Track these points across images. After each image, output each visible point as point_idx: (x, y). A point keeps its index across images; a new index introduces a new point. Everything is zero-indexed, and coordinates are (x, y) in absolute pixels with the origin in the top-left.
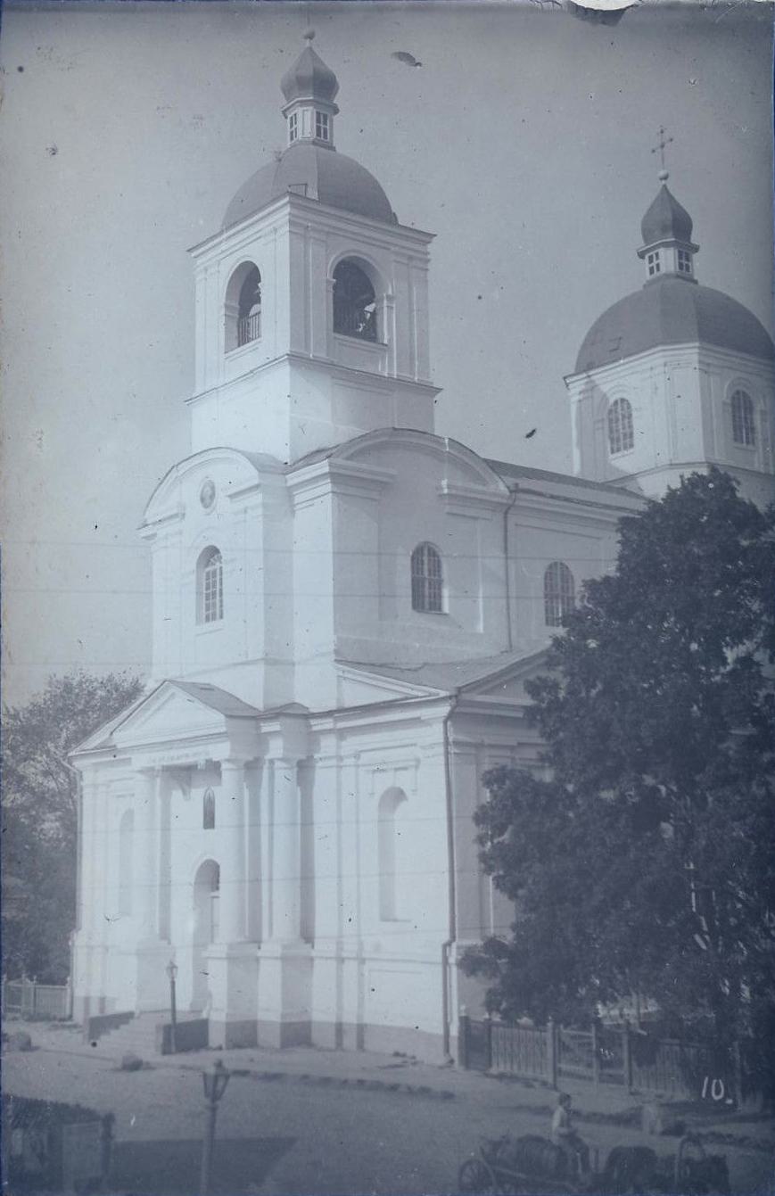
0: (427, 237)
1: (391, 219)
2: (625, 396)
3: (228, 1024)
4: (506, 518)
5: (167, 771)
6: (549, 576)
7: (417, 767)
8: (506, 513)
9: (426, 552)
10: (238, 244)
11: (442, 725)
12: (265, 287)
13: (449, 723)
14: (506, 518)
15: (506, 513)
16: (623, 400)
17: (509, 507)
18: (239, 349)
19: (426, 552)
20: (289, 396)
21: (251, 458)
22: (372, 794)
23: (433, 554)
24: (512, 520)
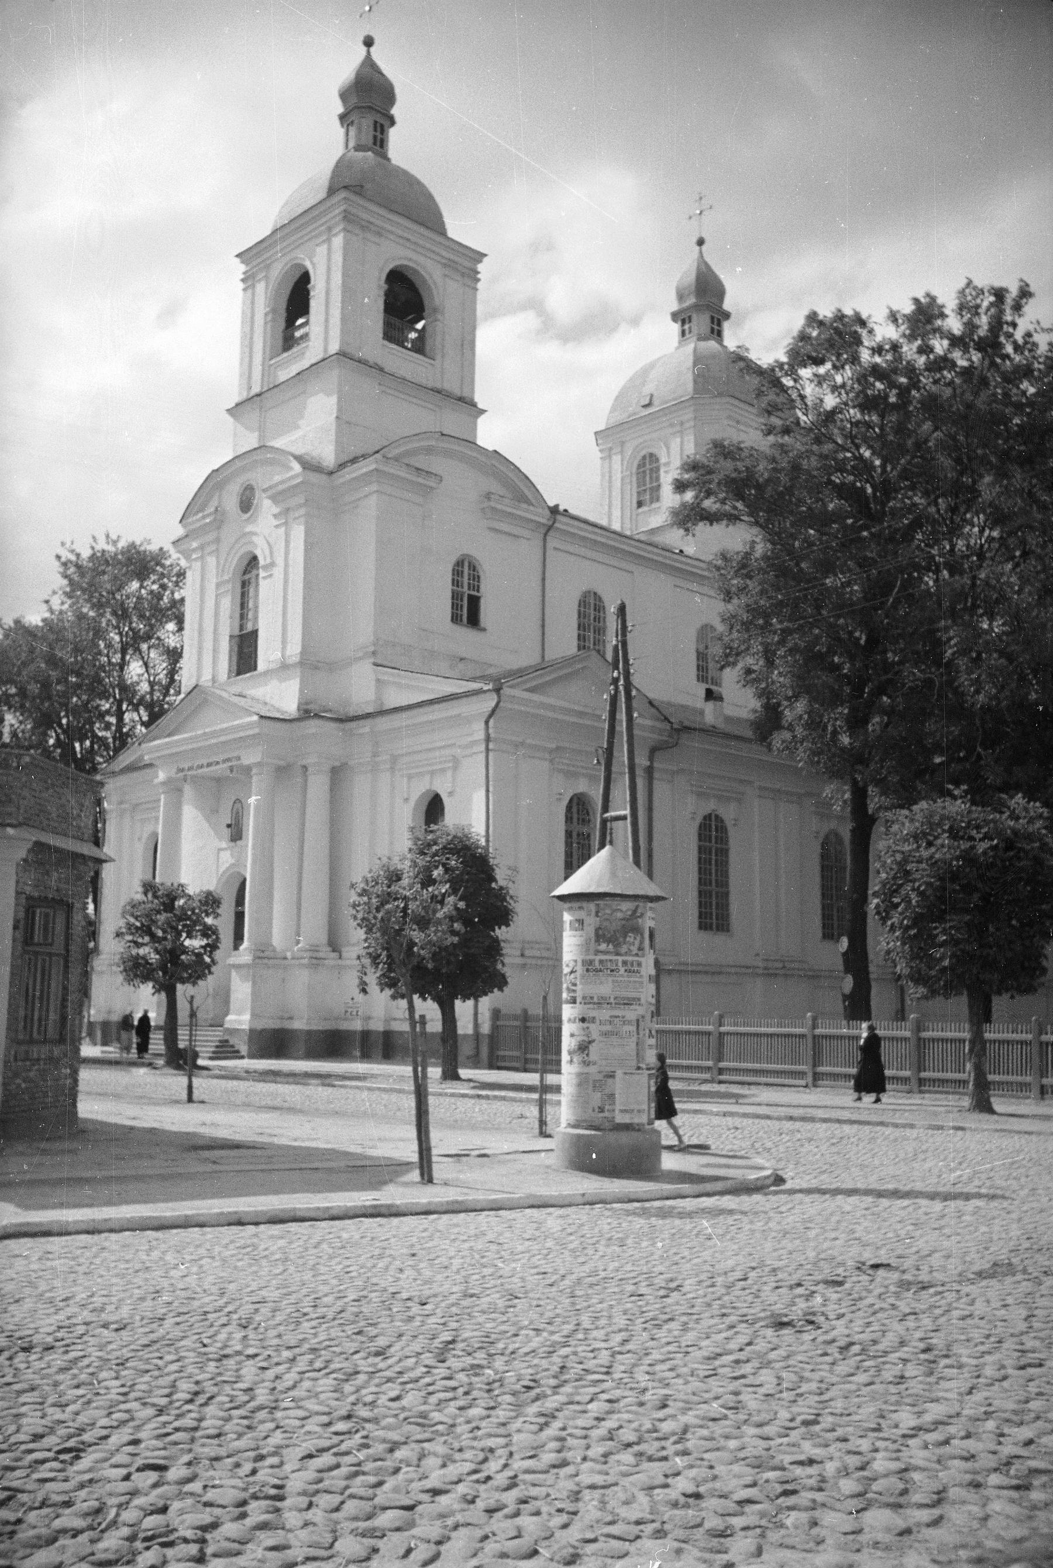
0: (480, 256)
1: (442, 232)
2: (650, 450)
3: (252, 1031)
4: (545, 540)
5: (353, 117)
6: (583, 603)
7: (455, 768)
8: (545, 535)
9: (466, 564)
10: (199, 659)
11: (482, 725)
12: (316, 304)
13: (491, 723)
14: (545, 540)
15: (545, 535)
16: (651, 455)
17: (550, 528)
18: (285, 355)
19: (466, 564)
20: (229, 826)
21: (298, 458)
22: (407, 800)
23: (473, 567)
24: (552, 542)
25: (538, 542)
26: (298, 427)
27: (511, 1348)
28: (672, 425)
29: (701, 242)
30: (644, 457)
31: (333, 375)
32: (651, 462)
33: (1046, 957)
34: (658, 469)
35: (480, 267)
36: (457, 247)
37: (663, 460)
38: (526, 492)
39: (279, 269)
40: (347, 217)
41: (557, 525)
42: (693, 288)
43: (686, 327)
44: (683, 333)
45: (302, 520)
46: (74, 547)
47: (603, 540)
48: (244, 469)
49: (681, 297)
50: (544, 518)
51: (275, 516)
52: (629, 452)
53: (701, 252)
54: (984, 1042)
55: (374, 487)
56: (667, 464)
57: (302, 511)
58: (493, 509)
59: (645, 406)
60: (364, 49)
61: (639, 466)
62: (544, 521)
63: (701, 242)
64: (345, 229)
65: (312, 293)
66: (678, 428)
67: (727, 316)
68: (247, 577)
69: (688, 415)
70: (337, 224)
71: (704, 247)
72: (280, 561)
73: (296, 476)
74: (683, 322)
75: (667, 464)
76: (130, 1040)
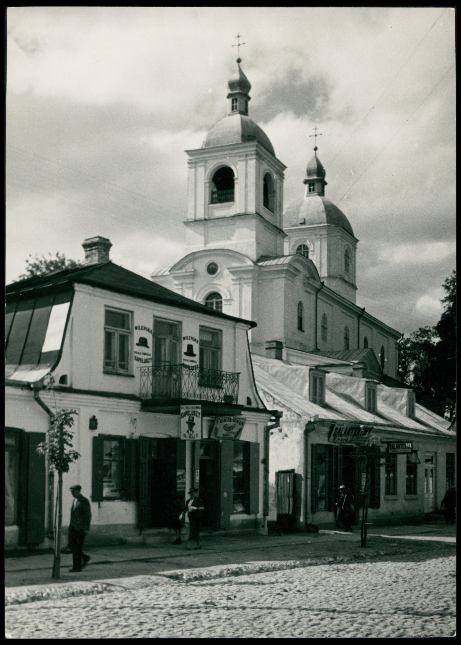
16: (304, 246)
26: (231, 239)
27: (345, 618)
28: (316, 235)
29: (316, 149)
30: (300, 246)
31: (254, 222)
32: (304, 249)
33: (65, 449)
34: (307, 252)
36: (280, 164)
37: (311, 248)
38: (315, 275)
41: (322, 290)
42: (316, 171)
43: (312, 187)
44: (310, 190)
45: (251, 284)
46: (37, 257)
47: (326, 292)
50: (318, 285)
52: (292, 243)
53: (316, 154)
55: (284, 275)
56: (313, 251)
58: (309, 283)
61: (298, 249)
62: (318, 287)
64: (256, 159)
66: (319, 237)
68: (209, 301)
69: (324, 232)
70: (252, 155)
71: (317, 151)
73: (250, 266)
74: (310, 185)
75: (313, 251)
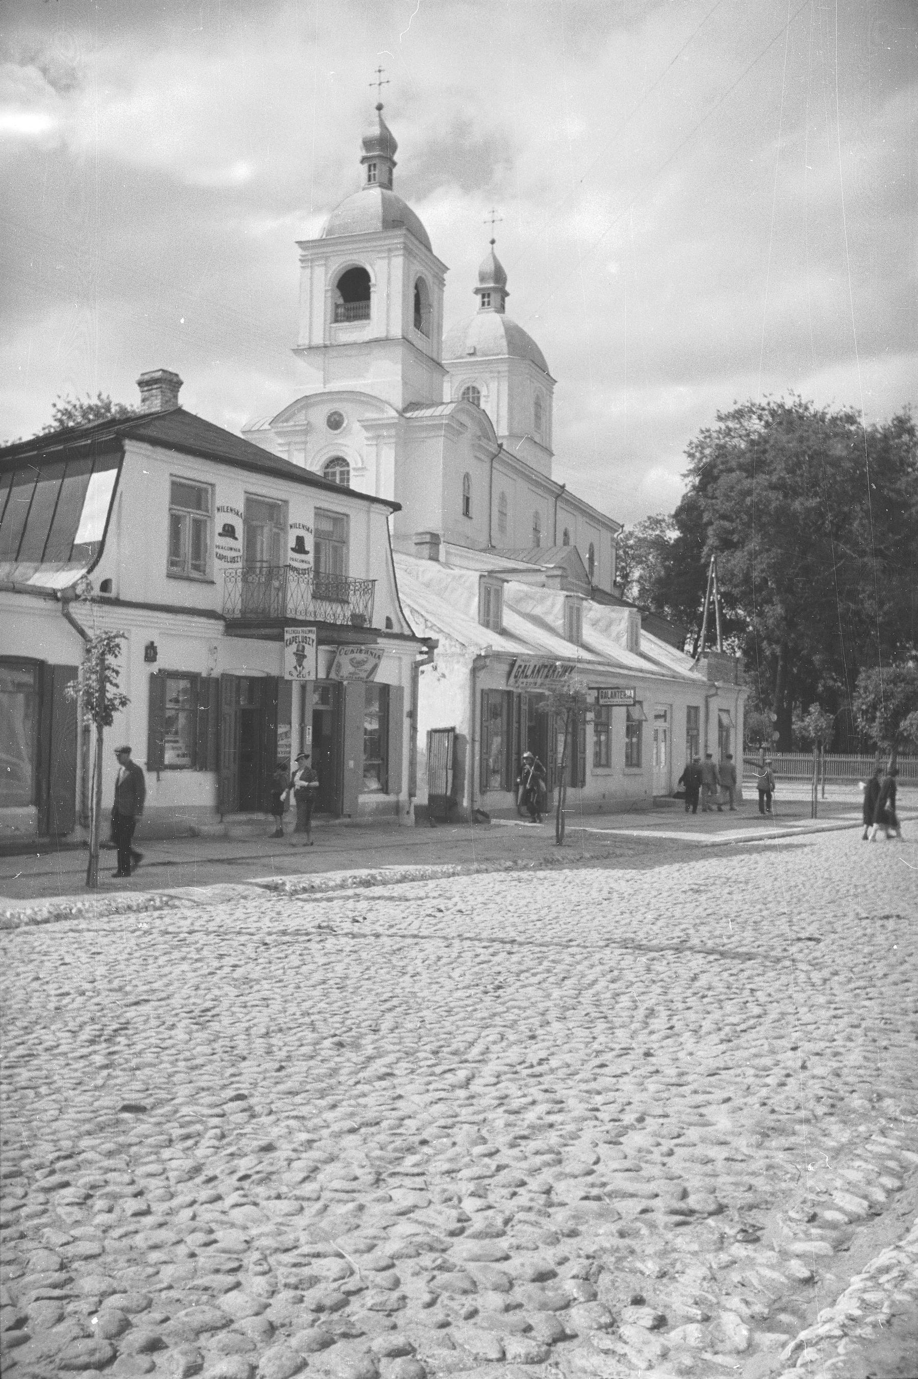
0: (447, 269)
17: (496, 456)
25: (487, 466)
29: (493, 242)
30: (468, 388)
31: (399, 351)
34: (479, 398)
35: (446, 276)
39: (338, 264)
40: (406, 248)
46: (69, 399)
48: (341, 400)
49: (482, 279)
51: (368, 439)
54: (37, 802)
57: (393, 440)
59: (471, 354)
60: (377, 112)
61: (464, 394)
63: (493, 242)
65: (372, 289)
67: (507, 294)
68: (330, 470)
69: (504, 368)
70: (397, 249)
72: (372, 469)
74: (483, 296)
76: (495, 762)
